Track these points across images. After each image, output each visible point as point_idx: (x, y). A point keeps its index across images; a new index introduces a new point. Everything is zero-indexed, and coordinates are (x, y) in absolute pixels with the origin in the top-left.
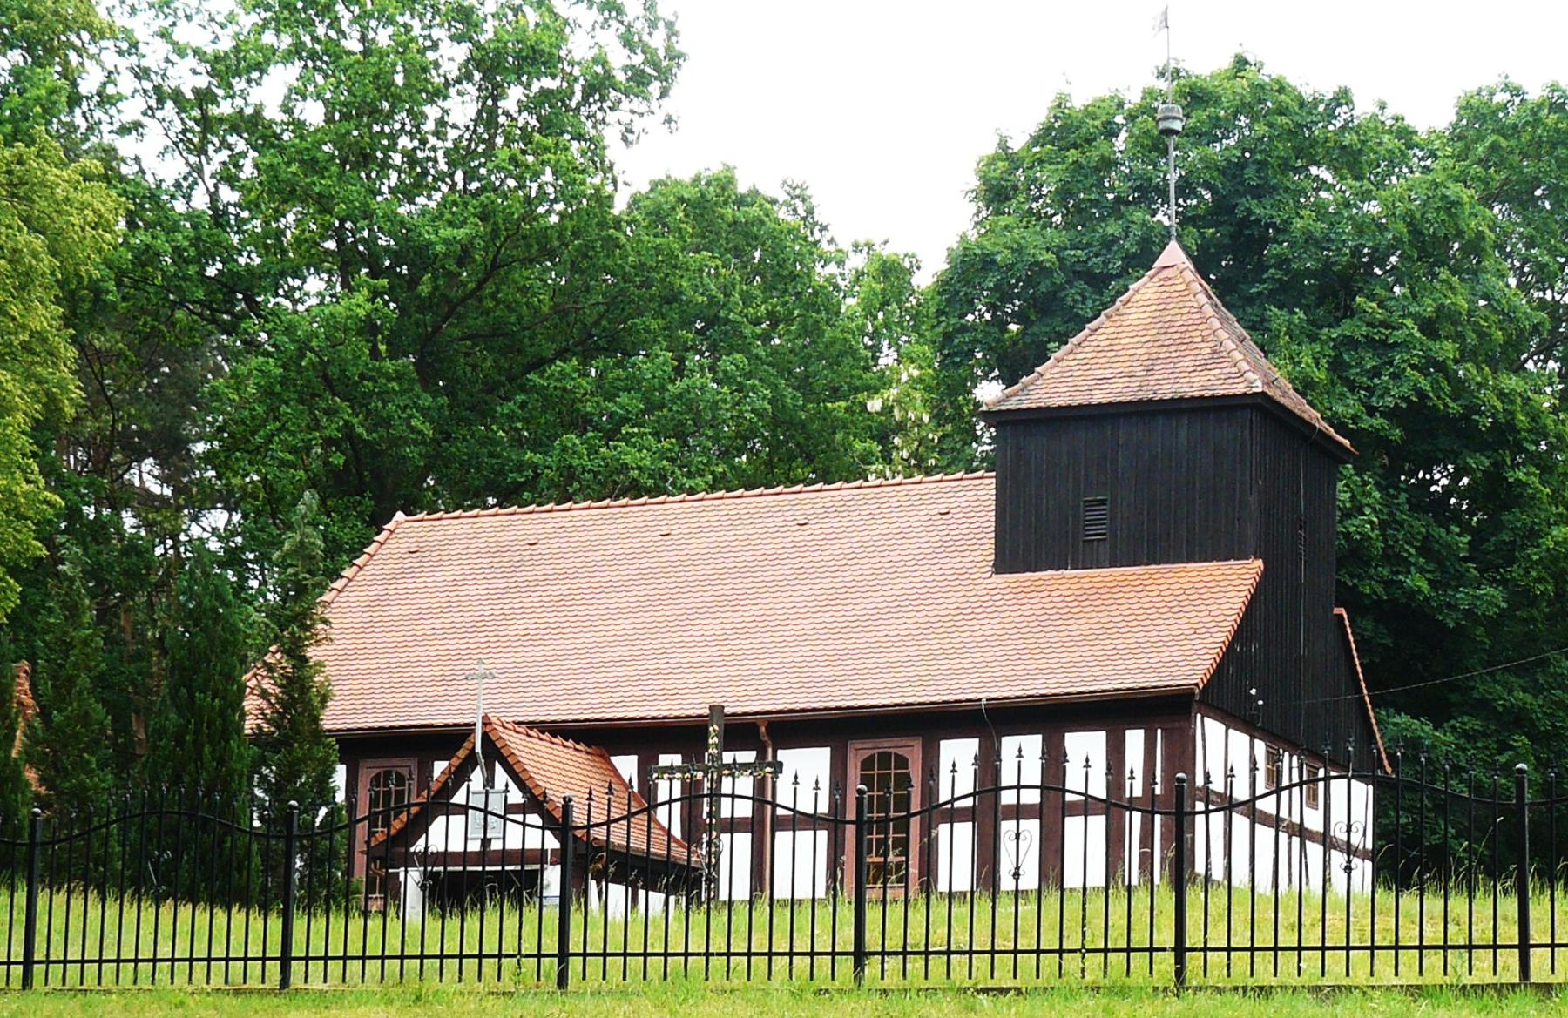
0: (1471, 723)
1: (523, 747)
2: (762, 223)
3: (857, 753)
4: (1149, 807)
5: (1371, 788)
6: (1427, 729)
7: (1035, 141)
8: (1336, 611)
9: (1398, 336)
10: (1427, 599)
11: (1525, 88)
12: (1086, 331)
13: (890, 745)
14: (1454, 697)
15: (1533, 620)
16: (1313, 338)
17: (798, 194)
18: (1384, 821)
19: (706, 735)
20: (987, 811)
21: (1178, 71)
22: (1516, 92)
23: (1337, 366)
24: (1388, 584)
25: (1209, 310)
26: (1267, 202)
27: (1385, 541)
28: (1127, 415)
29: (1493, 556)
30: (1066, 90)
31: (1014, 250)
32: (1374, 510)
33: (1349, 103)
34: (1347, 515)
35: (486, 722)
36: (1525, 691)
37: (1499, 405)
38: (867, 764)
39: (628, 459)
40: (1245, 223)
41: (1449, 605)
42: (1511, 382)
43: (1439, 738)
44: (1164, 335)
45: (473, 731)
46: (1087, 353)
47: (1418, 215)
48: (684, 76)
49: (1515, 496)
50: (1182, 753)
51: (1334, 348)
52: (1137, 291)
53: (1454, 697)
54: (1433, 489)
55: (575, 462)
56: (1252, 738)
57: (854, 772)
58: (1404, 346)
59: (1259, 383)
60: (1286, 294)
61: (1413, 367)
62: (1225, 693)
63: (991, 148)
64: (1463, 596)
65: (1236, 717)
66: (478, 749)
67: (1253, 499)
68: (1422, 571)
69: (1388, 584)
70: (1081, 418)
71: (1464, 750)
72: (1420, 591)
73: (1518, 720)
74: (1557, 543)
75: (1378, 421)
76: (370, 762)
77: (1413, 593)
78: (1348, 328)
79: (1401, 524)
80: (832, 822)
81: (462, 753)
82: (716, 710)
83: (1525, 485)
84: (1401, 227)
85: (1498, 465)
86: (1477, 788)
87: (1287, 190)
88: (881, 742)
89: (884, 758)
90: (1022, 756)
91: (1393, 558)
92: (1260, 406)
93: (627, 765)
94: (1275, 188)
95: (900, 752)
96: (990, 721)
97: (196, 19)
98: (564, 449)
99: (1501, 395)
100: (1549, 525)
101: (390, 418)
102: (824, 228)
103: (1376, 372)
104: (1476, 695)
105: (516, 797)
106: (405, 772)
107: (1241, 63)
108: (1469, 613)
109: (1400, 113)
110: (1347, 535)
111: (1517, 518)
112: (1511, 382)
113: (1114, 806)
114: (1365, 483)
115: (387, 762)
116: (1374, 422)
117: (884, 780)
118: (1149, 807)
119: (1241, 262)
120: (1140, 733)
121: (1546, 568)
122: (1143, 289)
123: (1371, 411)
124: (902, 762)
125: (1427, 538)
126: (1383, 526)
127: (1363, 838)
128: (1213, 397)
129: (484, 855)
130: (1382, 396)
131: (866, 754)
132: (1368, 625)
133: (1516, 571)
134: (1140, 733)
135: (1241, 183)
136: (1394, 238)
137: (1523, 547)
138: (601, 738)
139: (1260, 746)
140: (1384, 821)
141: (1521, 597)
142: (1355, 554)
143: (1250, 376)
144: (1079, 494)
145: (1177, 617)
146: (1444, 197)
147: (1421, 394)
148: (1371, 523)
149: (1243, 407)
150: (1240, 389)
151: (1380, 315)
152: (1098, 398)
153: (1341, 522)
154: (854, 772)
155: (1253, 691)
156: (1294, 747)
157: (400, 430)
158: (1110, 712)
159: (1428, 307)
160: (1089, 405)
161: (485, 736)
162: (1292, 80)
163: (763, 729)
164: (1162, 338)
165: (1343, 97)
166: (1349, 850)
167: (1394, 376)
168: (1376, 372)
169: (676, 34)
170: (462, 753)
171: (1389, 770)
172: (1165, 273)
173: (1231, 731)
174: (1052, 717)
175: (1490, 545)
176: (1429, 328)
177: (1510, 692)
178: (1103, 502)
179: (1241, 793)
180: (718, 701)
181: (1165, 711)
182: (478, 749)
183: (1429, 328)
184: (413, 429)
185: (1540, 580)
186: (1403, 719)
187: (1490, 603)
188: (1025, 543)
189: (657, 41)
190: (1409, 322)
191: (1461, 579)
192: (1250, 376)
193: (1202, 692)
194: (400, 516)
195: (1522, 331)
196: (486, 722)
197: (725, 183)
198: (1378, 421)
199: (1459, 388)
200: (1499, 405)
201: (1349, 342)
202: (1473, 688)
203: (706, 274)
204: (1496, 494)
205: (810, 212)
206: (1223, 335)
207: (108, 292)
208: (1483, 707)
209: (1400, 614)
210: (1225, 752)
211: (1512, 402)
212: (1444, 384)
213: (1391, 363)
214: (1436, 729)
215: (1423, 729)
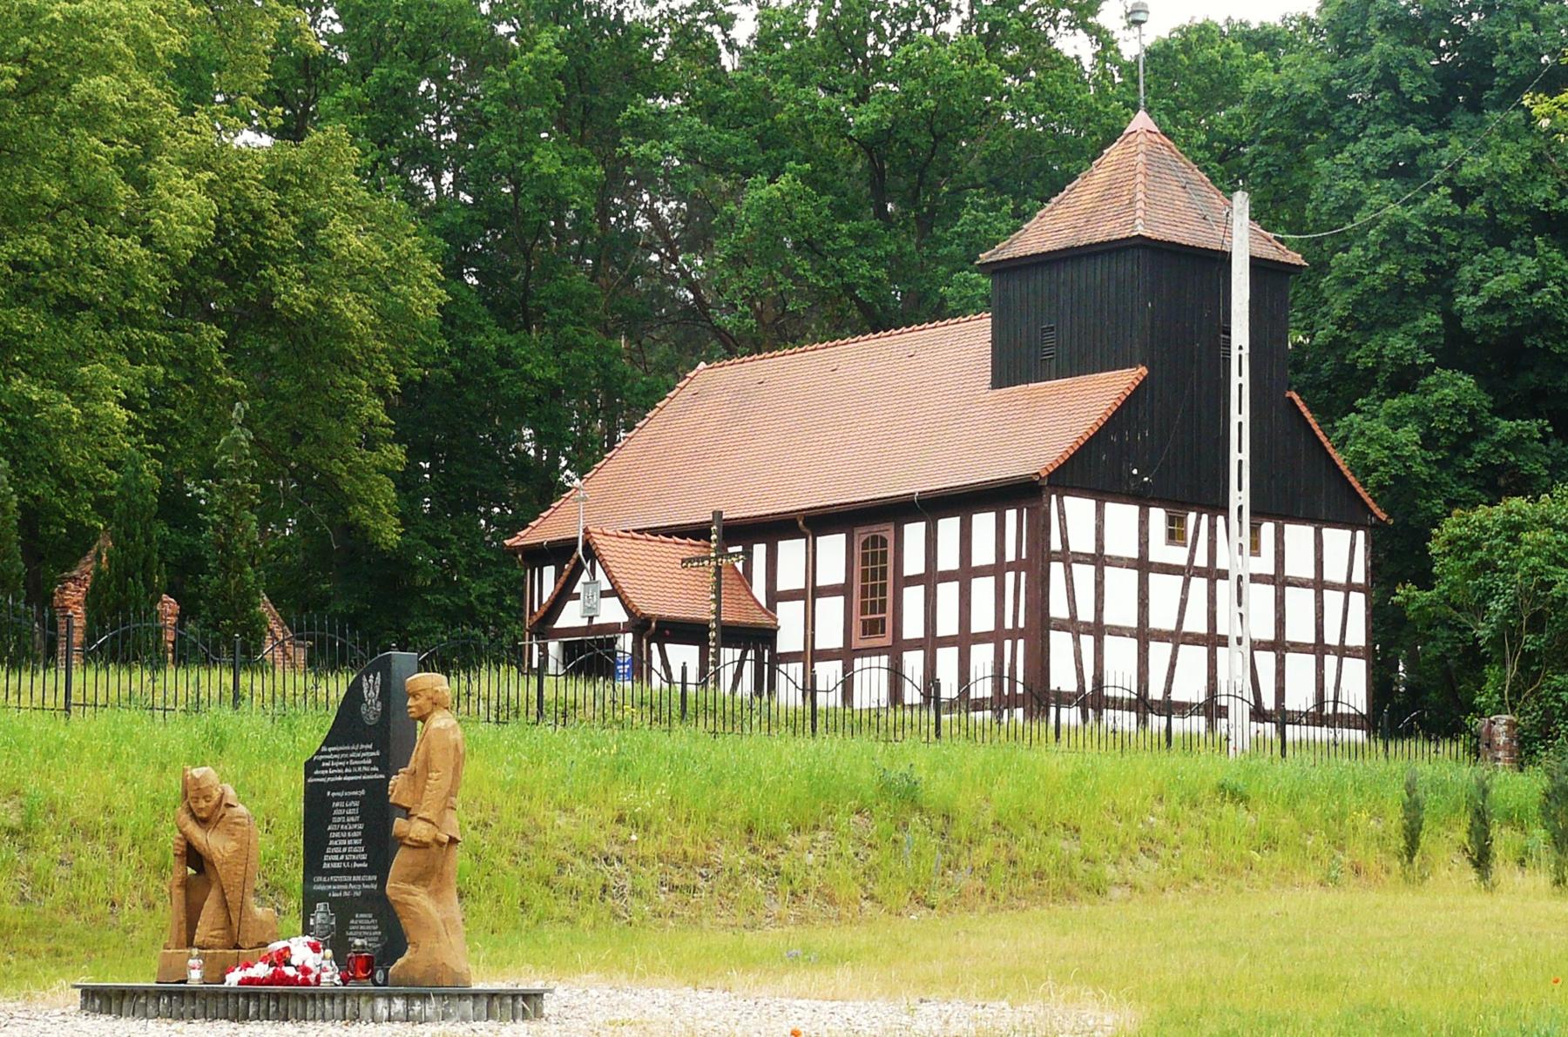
28: (1102, 253)
56: (1354, 532)
57: (858, 551)
70: (1015, 269)
89: (875, 538)
105: (606, 586)
106: (884, 534)
113: (997, 570)
118: (1016, 566)
120: (1014, 512)
124: (884, 542)
129: (589, 629)
134: (1014, 512)
149: (1127, 248)
154: (858, 551)
172: (1131, 137)
178: (1052, 329)
180: (720, 508)
188: (1012, 366)
194: (702, 365)
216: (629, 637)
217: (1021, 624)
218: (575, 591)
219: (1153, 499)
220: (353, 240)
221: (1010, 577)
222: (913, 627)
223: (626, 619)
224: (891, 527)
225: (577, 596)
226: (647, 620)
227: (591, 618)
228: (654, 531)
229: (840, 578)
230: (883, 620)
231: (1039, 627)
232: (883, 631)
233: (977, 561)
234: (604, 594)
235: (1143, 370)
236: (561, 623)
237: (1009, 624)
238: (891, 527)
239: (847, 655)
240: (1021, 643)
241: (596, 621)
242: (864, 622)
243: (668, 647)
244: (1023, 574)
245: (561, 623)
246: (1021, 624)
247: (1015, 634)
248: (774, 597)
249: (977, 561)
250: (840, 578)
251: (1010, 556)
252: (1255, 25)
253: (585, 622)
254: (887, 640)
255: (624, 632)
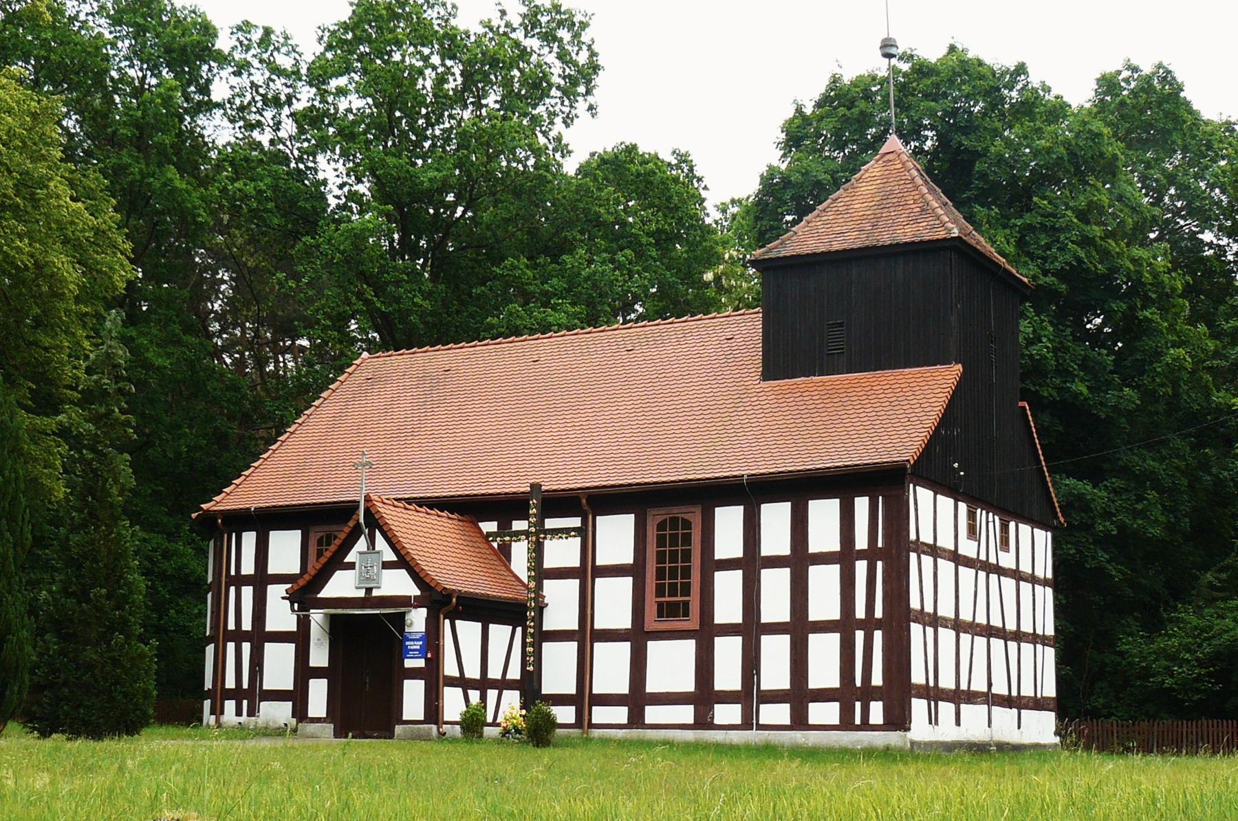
0: (1118, 483)
1: (393, 516)
2: (655, 173)
3: (655, 517)
4: (871, 555)
5: (1049, 534)
6: (1088, 488)
7: (819, 105)
8: (1020, 404)
9: (1061, 222)
10: (1086, 399)
11: (1141, 67)
12: (829, 201)
13: (679, 512)
14: (1106, 466)
15: (1157, 413)
16: (1004, 227)
17: (683, 159)
18: (1059, 552)
19: (528, 507)
20: (752, 563)
21: (912, 56)
22: (1135, 69)
23: (1021, 243)
24: (1060, 389)
25: (919, 181)
26: (973, 137)
27: (1057, 361)
29: (1132, 368)
30: (839, 71)
31: (803, 175)
32: (1049, 340)
33: (1026, 73)
34: (1030, 342)
35: (368, 499)
36: (1154, 460)
37: (1132, 267)
38: (661, 526)
39: (550, 319)
40: (958, 151)
41: (1101, 404)
42: (1137, 252)
43: (1097, 494)
44: (885, 201)
45: (357, 507)
46: (830, 216)
47: (1073, 142)
48: (600, 80)
49: (1145, 328)
50: (897, 518)
51: (1019, 232)
52: (866, 171)
53: (1106, 466)
54: (1088, 326)
55: (519, 322)
56: (956, 501)
58: (1068, 228)
59: (956, 231)
60: (983, 198)
61: (1073, 242)
62: (939, 466)
63: (790, 113)
64: (1111, 396)
65: (941, 486)
66: (362, 521)
67: (953, 318)
68: (1082, 380)
69: (1060, 389)
71: (1113, 502)
72: (1081, 394)
73: (1152, 479)
74: (1174, 360)
75: (1050, 279)
76: (318, 528)
77: (1077, 395)
78: (1028, 218)
79: (1068, 349)
80: (634, 571)
81: (351, 524)
82: (535, 487)
83: (1151, 321)
84: (1062, 149)
85: (1132, 308)
86: (1122, 527)
87: (985, 129)
88: (672, 512)
89: (674, 520)
90: (776, 519)
91: (1063, 372)
92: (956, 248)
93: (489, 527)
94: (977, 128)
95: (686, 516)
96: (750, 493)
97: (284, 50)
98: (511, 314)
99: (1134, 261)
100: (1168, 348)
101: (401, 297)
102: (699, 180)
103: (1048, 247)
104: (1120, 463)
105: (390, 556)
107: (952, 49)
108: (1115, 408)
109: (1060, 93)
110: (1031, 356)
111: (1148, 343)
112: (1137, 252)
114: (1043, 321)
115: (327, 528)
116: (1047, 279)
117: (674, 538)
118: (871, 555)
119: (953, 170)
120: (244, 628)
121: (1167, 377)
122: (872, 169)
123: (1045, 273)
124: (687, 524)
125: (1085, 358)
126: (1055, 350)
127: (1044, 568)
128: (921, 242)
129: (368, 601)
130: (1052, 263)
131: (659, 519)
132: (1046, 418)
133: (1146, 380)
134: (244, 628)
135: (952, 115)
136: (1058, 158)
137: (1151, 363)
138: (469, 508)
139: (963, 507)
140: (1059, 552)
141: (1149, 396)
142: (1036, 370)
143: (950, 225)
144: (824, 316)
145: (897, 410)
146: (1090, 131)
147: (1079, 260)
148: (1047, 347)
150: (942, 234)
151: (1050, 209)
152: (836, 246)
153: (1026, 348)
154: (652, 534)
155: (956, 465)
156: (990, 507)
157: (406, 305)
158: (841, 483)
159: (1082, 202)
160: (829, 252)
161: (367, 510)
162: (988, 61)
163: (584, 501)
164: (889, 203)
165: (1021, 69)
166: (1033, 579)
167: (1060, 249)
168: (1048, 247)
169: (596, 54)
170: (351, 524)
171: (1062, 520)
173: (939, 496)
174: (798, 488)
175: (1128, 363)
176: (1083, 216)
177: (1144, 460)
178: (841, 325)
179: (945, 542)
181: (885, 483)
182: (362, 521)
183: (1083, 216)
184: (415, 304)
185: (1163, 385)
186: (1071, 482)
187: (1130, 401)
188: (784, 358)
189: (583, 58)
190: (1069, 213)
191: (1109, 384)
192: (950, 225)
193: (913, 466)
195: (1145, 220)
196: (368, 499)
197: (631, 149)
198: (1050, 279)
199: (1105, 254)
200: (1132, 267)
201: (1030, 228)
202: (1119, 459)
203: (632, 213)
204: (1131, 328)
205: (691, 170)
206: (929, 197)
207: (199, 215)
208: (1125, 471)
209: (1068, 412)
210: (934, 514)
211: (1141, 265)
212: (1094, 254)
213: (1058, 241)
214: (1094, 487)
215: (1085, 487)
216: (423, 612)
217: (879, 614)
218: (348, 559)
219: (964, 493)
220: (66, 203)
221: (861, 567)
222: (728, 608)
223: (418, 593)
224: (698, 510)
225: (351, 566)
226: (447, 595)
227: (369, 590)
228: (409, 501)
229: (627, 558)
230: (686, 604)
231: (898, 619)
232: (686, 614)
233: (767, 549)
234: (387, 565)
235: (948, 376)
236: (327, 592)
237: (860, 613)
238: (698, 510)
239: (638, 637)
240: (878, 635)
241: (375, 593)
242: (660, 605)
243: (458, 622)
244: (880, 564)
245: (327, 592)
246: (879, 614)
247: (869, 625)
248: (541, 573)
249: (767, 549)
250: (627, 558)
251: (861, 542)
252: (970, 55)
253: (361, 594)
254: (652, 621)
255: (416, 607)
